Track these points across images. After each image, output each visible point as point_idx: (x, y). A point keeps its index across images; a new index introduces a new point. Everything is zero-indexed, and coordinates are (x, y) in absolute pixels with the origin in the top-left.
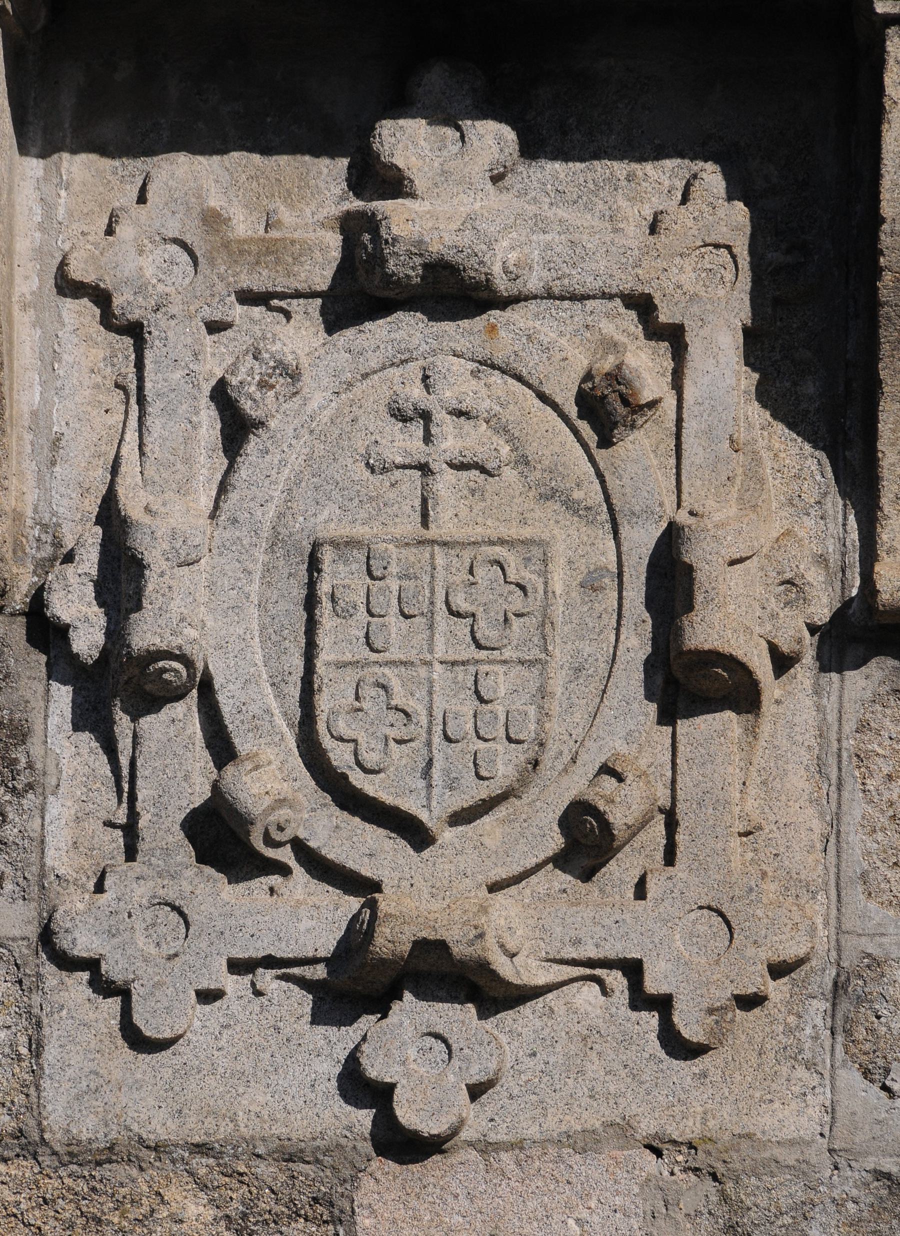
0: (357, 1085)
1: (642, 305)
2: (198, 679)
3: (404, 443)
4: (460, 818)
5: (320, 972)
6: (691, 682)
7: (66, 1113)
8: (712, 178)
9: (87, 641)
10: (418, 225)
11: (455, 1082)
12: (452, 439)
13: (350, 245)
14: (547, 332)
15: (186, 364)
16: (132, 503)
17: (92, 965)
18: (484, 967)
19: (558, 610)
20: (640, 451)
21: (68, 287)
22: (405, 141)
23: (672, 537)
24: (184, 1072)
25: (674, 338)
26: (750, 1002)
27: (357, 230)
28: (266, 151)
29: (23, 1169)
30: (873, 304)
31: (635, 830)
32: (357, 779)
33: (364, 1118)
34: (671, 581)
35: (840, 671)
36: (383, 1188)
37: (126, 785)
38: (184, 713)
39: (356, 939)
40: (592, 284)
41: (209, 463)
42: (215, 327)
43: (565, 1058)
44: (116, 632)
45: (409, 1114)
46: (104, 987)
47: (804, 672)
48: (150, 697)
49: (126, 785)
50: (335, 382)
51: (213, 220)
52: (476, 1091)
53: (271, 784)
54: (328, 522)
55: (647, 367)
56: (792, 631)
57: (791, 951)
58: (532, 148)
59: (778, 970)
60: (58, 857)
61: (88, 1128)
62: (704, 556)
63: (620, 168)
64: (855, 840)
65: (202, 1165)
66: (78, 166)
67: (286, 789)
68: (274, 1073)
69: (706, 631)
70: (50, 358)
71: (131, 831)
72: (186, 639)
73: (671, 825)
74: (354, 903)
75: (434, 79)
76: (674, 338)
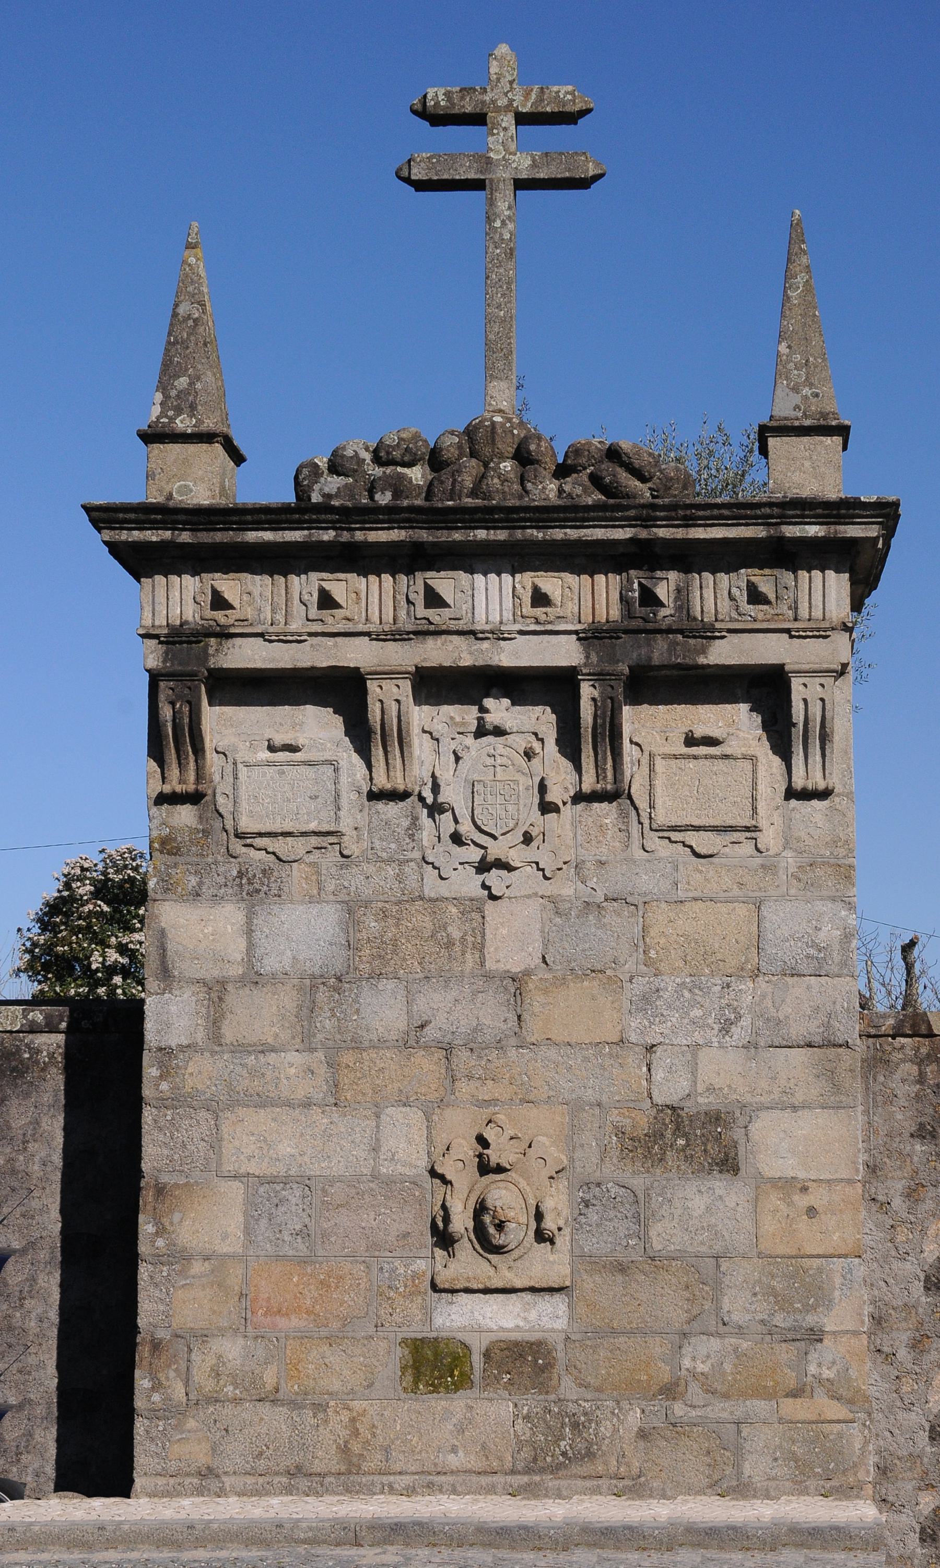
0: (484, 886)
1: (536, 734)
2: (359, 536)
3: (490, 761)
4: (503, 834)
5: (477, 865)
6: (547, 808)
7: (428, 892)
8: (548, 709)
9: (430, 801)
10: (492, 719)
11: (504, 886)
12: (499, 760)
13: (479, 723)
14: (518, 740)
15: (448, 746)
16: (437, 774)
17: (432, 863)
18: (508, 863)
19: (521, 794)
20: (536, 761)
21: (424, 731)
22: (489, 702)
23: (543, 779)
24: (451, 884)
25: (542, 740)
26: (559, 869)
27: (480, 719)
28: (462, 705)
29: (421, 903)
30: (580, 734)
31: (537, 837)
32: (483, 827)
33: (486, 892)
34: (542, 788)
35: (306, 573)
36: (490, 906)
37: (438, 828)
38: (449, 814)
39: (484, 858)
40: (526, 730)
41: (452, 765)
42: (453, 739)
43: (523, 881)
44: (435, 799)
45: (494, 892)
46: (435, 868)
47: (569, 805)
48: (442, 811)
49: (438, 828)
50: (476, 748)
51: (452, 718)
52: (507, 887)
53: (466, 828)
54: (476, 777)
55: (537, 746)
56: (567, 797)
57: (567, 860)
58: (513, 704)
59: (565, 863)
60: (425, 843)
61: (433, 895)
62: (548, 782)
63: (531, 708)
64: (579, 837)
65: (455, 901)
66: (426, 708)
67: (469, 829)
68: (468, 884)
69: (549, 798)
70: (421, 745)
71: (439, 837)
72: (449, 800)
73: (544, 835)
74: (483, 851)
75: (494, 691)
76: (542, 740)
